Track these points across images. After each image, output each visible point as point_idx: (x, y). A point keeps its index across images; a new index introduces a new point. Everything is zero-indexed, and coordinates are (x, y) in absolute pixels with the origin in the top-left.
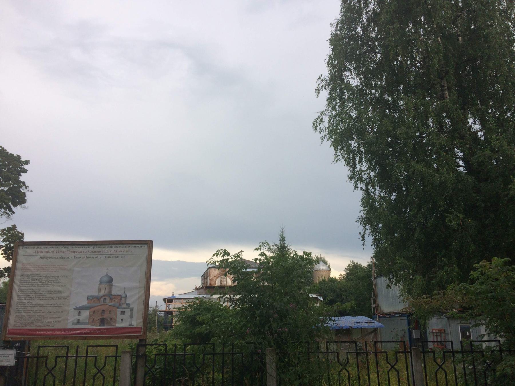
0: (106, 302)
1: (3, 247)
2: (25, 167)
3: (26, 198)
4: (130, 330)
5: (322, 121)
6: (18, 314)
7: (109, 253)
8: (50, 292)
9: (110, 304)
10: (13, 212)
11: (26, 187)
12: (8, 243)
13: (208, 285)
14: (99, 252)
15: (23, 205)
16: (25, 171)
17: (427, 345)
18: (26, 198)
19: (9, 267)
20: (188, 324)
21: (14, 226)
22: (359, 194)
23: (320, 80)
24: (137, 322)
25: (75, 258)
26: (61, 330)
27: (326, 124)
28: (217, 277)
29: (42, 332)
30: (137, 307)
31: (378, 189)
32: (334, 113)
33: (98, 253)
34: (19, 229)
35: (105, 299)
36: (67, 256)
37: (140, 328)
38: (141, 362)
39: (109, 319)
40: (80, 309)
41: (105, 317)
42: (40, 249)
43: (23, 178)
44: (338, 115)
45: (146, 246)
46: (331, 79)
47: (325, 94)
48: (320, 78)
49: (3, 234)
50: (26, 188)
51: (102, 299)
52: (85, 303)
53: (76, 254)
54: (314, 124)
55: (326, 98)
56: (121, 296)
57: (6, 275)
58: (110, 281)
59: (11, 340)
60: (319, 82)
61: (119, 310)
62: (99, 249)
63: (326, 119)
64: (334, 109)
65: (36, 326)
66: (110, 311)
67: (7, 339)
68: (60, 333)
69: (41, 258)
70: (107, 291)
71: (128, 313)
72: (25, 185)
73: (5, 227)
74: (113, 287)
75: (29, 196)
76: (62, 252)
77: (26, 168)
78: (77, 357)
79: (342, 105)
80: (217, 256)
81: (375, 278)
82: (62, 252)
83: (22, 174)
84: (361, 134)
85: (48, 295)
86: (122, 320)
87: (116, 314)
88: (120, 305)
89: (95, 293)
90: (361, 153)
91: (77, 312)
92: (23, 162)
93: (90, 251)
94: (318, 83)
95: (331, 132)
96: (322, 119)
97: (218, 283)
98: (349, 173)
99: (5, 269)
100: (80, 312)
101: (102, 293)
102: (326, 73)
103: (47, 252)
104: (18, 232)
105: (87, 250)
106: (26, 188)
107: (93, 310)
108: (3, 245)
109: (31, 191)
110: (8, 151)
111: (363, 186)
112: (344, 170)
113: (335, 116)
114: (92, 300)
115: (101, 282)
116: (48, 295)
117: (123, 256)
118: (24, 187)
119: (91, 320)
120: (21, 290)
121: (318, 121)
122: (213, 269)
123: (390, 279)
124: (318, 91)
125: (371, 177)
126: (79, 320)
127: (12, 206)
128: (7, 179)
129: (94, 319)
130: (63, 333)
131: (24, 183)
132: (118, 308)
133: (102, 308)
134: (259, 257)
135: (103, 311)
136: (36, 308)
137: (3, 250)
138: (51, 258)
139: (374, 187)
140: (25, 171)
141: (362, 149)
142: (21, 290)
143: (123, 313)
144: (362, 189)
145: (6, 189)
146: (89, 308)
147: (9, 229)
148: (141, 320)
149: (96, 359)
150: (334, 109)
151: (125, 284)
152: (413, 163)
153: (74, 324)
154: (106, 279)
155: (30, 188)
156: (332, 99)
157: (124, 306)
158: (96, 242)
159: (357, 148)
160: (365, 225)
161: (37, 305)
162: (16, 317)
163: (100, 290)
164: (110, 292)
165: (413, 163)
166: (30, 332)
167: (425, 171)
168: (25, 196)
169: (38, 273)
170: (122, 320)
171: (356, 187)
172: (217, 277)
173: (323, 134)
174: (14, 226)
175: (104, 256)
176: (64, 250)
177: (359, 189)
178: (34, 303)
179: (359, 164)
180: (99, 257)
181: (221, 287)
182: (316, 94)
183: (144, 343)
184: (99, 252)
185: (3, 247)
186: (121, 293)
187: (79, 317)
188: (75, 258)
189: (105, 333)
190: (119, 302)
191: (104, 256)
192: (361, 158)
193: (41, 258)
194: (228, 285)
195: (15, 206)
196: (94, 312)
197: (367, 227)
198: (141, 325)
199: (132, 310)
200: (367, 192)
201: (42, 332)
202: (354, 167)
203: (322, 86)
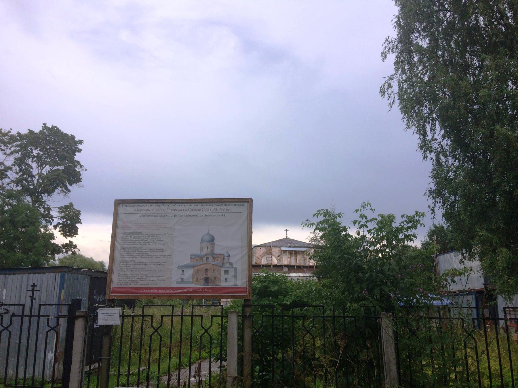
0: (210, 260)
1: (60, 224)
2: (80, 146)
3: (81, 177)
4: (235, 290)
5: (390, 86)
6: (121, 273)
7: (209, 211)
8: (152, 250)
9: (213, 263)
10: (69, 191)
11: (81, 166)
12: (65, 220)
13: (254, 263)
14: (199, 210)
15: (78, 184)
16: (80, 151)
17: (499, 321)
18: (81, 177)
19: (66, 244)
20: (255, 296)
21: (71, 204)
22: (429, 165)
23: (387, 42)
24: (241, 282)
25: (175, 216)
26: (165, 289)
27: (395, 89)
28: (262, 256)
29: (146, 291)
30: (242, 267)
31: (450, 158)
32: (404, 76)
33: (198, 212)
34: (76, 207)
35: (208, 258)
36: (167, 214)
37: (246, 288)
38: (247, 323)
39: (213, 279)
40: (183, 268)
41: (209, 276)
42: (140, 207)
43: (78, 157)
44: (409, 79)
45: (246, 204)
46: (400, 40)
47: (392, 58)
48: (387, 40)
49: (61, 212)
50: (81, 167)
51: (205, 258)
52: (188, 261)
53: (176, 212)
54: (381, 90)
55: (394, 62)
56: (223, 255)
57: (64, 251)
58: (212, 240)
59: (116, 298)
60: (386, 44)
61: (223, 270)
62: (200, 207)
63: (395, 84)
64: (403, 72)
65: (139, 284)
66: (214, 270)
67: (111, 298)
68: (164, 291)
69: (142, 216)
70: (209, 250)
71: (232, 272)
72: (80, 164)
73: (63, 205)
74: (215, 246)
75: (84, 175)
76: (162, 210)
77: (80, 148)
78: (172, 316)
79: (411, 69)
80: (317, 216)
81: (437, 256)
82: (162, 210)
83: (76, 153)
84: (434, 99)
85: (151, 254)
86: (226, 279)
87: (220, 274)
88: (223, 264)
89: (197, 252)
90: (433, 120)
91: (180, 271)
92: (77, 141)
93: (190, 210)
94: (384, 46)
95: (401, 96)
96: (390, 84)
97: (263, 262)
98: (419, 141)
99: (63, 245)
100: (183, 271)
101: (205, 252)
102: (393, 34)
103: (147, 210)
104: (75, 209)
105: (187, 208)
106: (81, 167)
107: (196, 268)
108: (61, 222)
109: (86, 170)
110: (62, 131)
111: (433, 155)
112: (415, 139)
113: (405, 81)
114: (194, 258)
115: (203, 241)
116: (151, 254)
117: (224, 214)
118: (79, 166)
119: (195, 279)
120: (123, 248)
121: (386, 86)
122: (259, 248)
123: (463, 254)
124: (384, 55)
125: (442, 146)
126: (182, 279)
127: (68, 185)
128: (63, 158)
129: (197, 278)
130: (167, 291)
131: (78, 162)
132: (221, 267)
133: (205, 267)
134: (359, 219)
135: (207, 270)
136: (140, 267)
137: (61, 227)
138: (152, 216)
139: (446, 156)
140: (80, 151)
141: (434, 115)
142: (123, 248)
143: (226, 272)
144: (432, 159)
145: (62, 168)
146: (193, 267)
147: (67, 207)
148: (245, 280)
149: (202, 318)
150: (403, 72)
151: (227, 243)
152: (498, 127)
153: (178, 283)
154: (207, 238)
155: (85, 167)
156: (400, 62)
157: (228, 265)
158: (195, 200)
159: (429, 114)
160: (435, 198)
161: (140, 263)
162: (119, 276)
163: (202, 249)
164: (213, 250)
165: (498, 127)
166: (135, 291)
167: (512, 135)
168: (80, 175)
169: (139, 231)
170: (226, 279)
171: (425, 157)
172: (262, 256)
173: (391, 100)
174: (71, 204)
175: (204, 215)
176: (164, 208)
177: (428, 159)
178: (137, 261)
179: (431, 131)
180: (199, 215)
181: (268, 266)
182: (381, 58)
183: (249, 304)
184: (199, 210)
185: (60, 224)
186: (223, 252)
187: (182, 276)
188: (175, 216)
189: (208, 292)
190: (223, 261)
191: (204, 215)
192: (433, 125)
193: (142, 216)
194: (273, 264)
195: (71, 185)
196: (198, 270)
197: (437, 200)
198: (245, 285)
199: (236, 269)
200: (438, 162)
201: (146, 291)
202: (424, 134)
203: (389, 49)
